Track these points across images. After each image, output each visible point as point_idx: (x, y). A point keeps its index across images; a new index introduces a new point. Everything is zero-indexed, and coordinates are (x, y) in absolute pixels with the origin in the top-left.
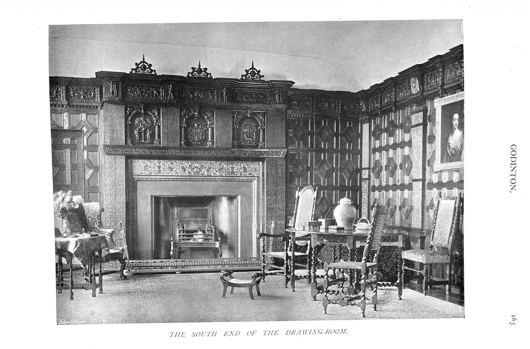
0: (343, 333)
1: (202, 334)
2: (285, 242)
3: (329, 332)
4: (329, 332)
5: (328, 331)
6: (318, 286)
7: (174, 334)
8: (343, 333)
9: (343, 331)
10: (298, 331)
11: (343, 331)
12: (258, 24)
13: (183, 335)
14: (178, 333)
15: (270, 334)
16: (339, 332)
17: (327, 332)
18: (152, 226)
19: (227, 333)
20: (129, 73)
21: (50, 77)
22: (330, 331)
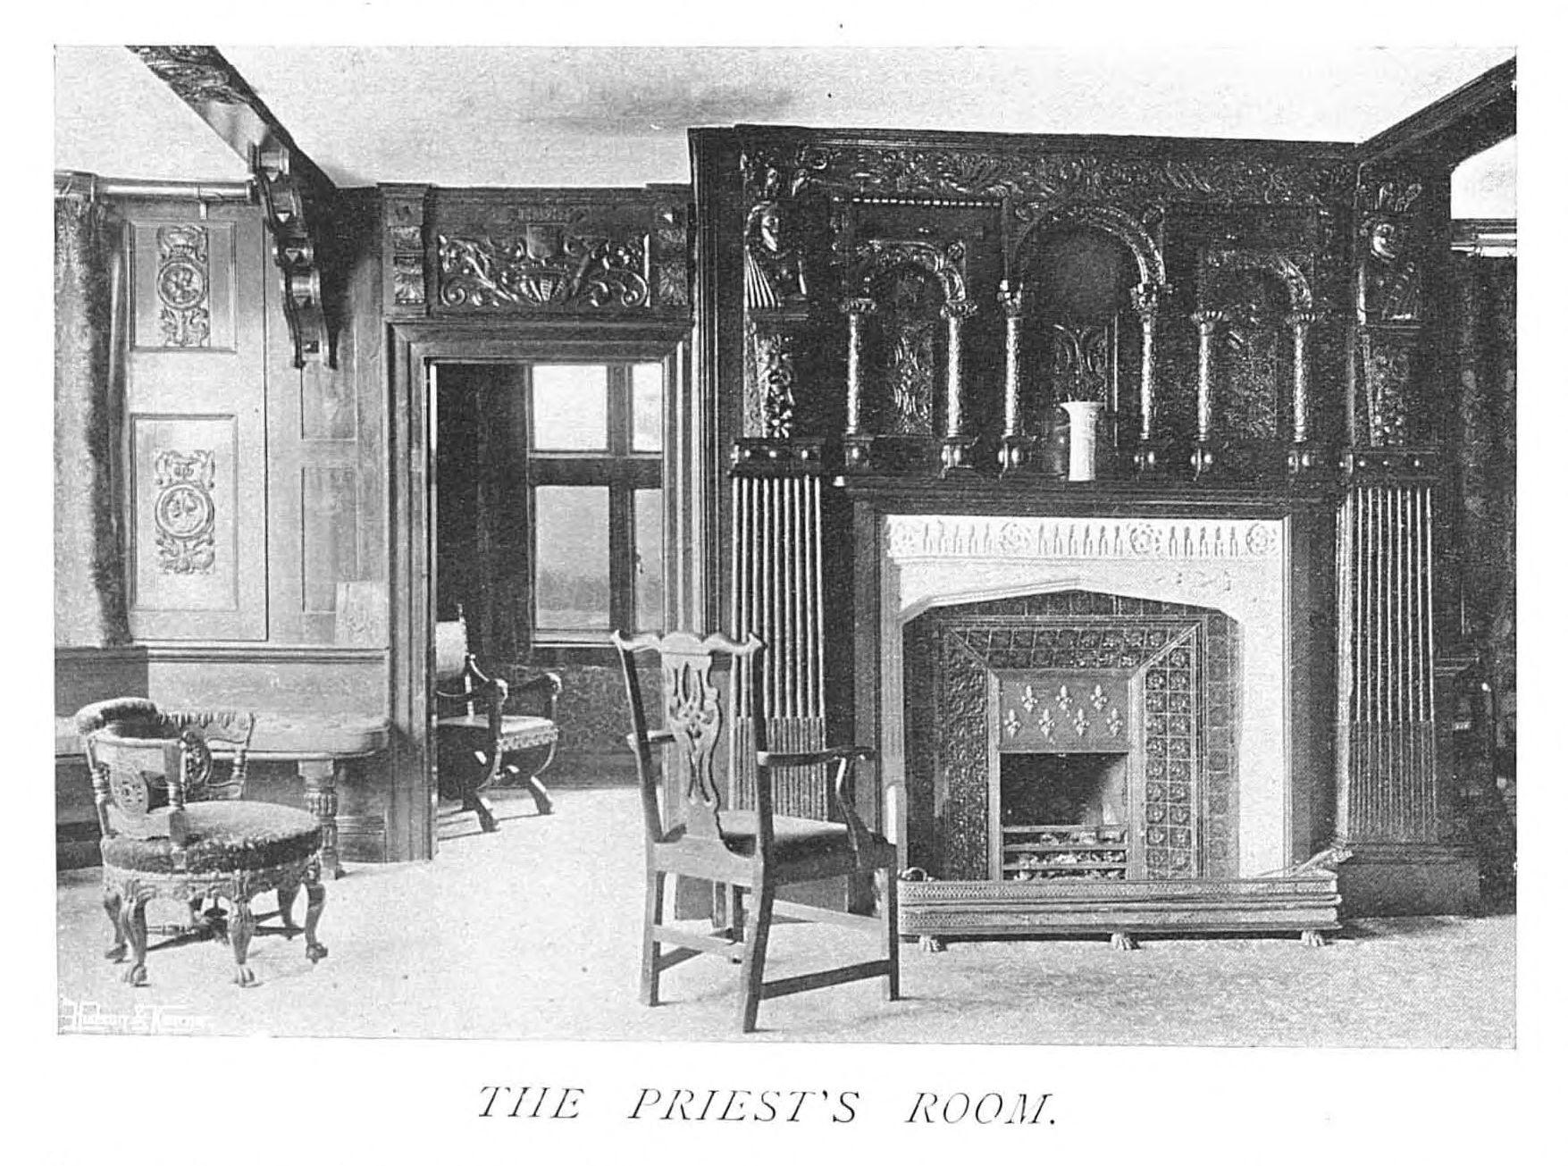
19: (571, 1096)
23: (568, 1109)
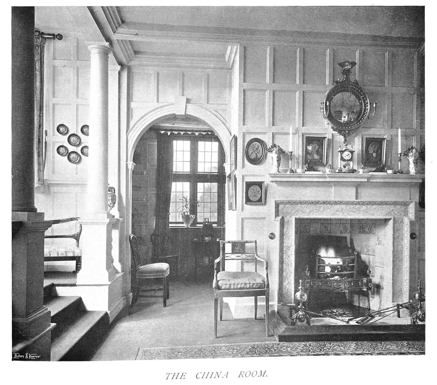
0: (262, 375)
2: (53, 325)
3: (244, 375)
4: (244, 375)
5: (242, 373)
6: (270, 311)
7: (171, 376)
8: (262, 375)
9: (263, 374)
10: (224, 373)
11: (263, 374)
12: (12, 283)
13: (183, 377)
14: (176, 375)
15: (175, 377)
16: (258, 375)
17: (241, 375)
18: (318, 134)
19: (183, 375)
20: (53, 225)
21: (12, 222)
22: (245, 374)
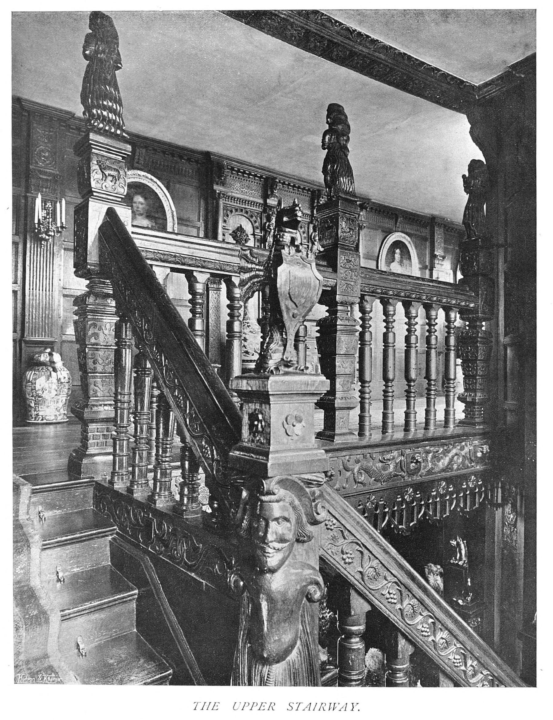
1: (333, 707)
17: (271, 707)
19: (216, 704)
23: (215, 708)
